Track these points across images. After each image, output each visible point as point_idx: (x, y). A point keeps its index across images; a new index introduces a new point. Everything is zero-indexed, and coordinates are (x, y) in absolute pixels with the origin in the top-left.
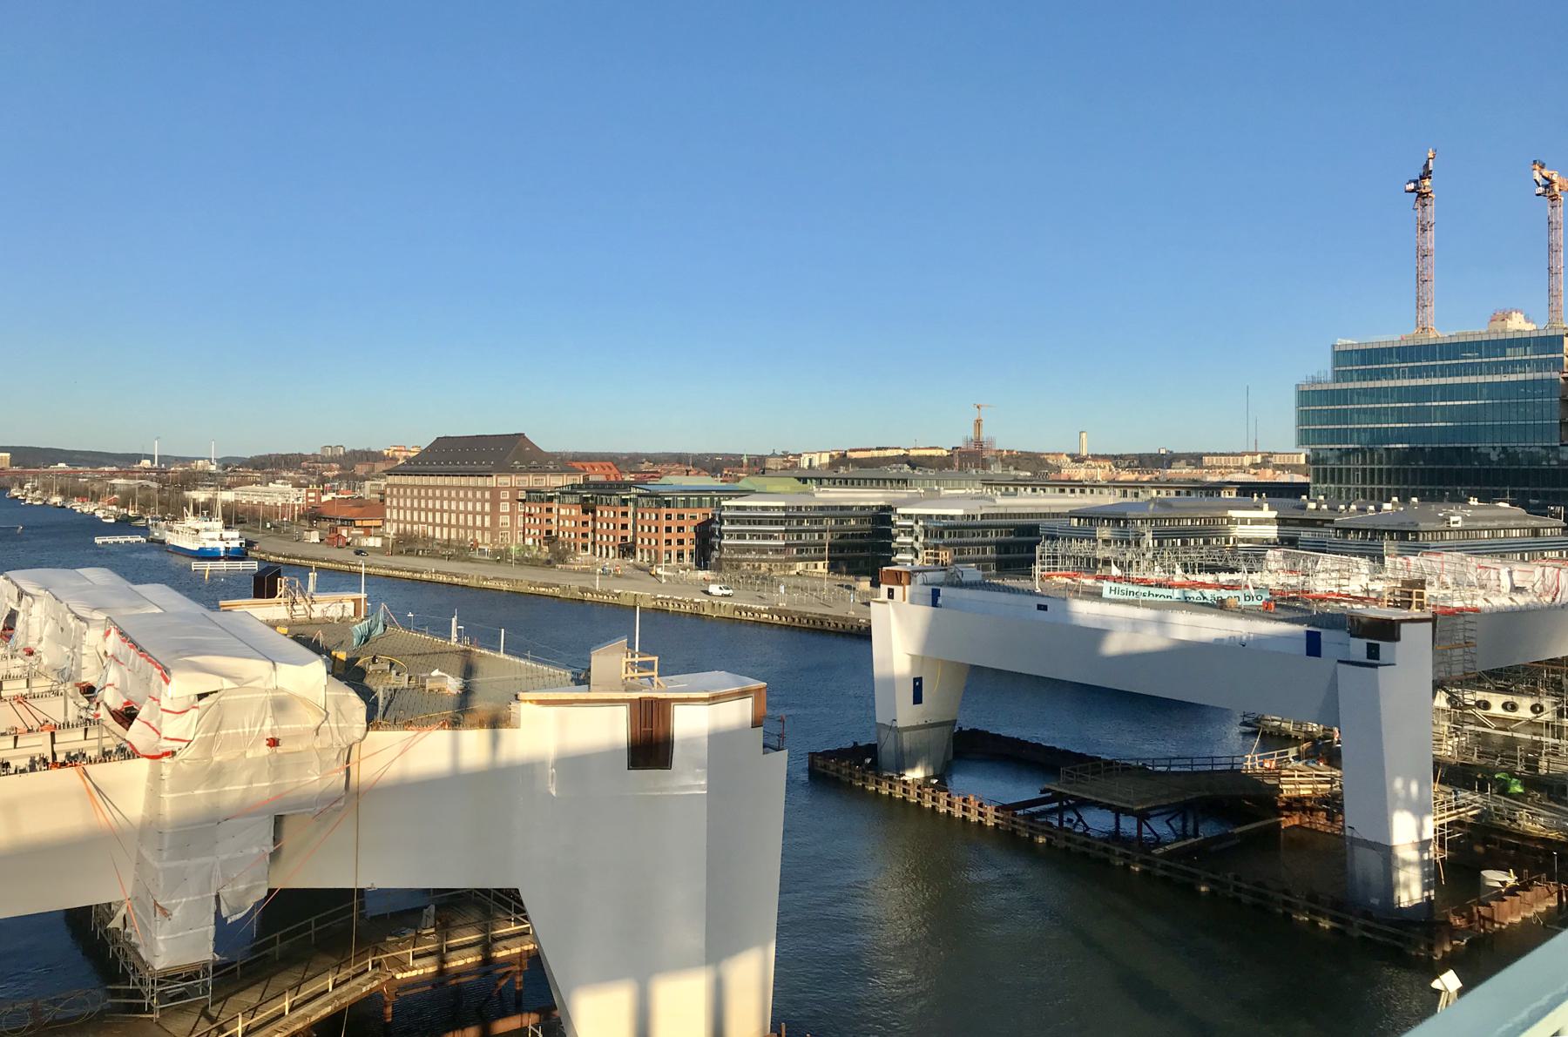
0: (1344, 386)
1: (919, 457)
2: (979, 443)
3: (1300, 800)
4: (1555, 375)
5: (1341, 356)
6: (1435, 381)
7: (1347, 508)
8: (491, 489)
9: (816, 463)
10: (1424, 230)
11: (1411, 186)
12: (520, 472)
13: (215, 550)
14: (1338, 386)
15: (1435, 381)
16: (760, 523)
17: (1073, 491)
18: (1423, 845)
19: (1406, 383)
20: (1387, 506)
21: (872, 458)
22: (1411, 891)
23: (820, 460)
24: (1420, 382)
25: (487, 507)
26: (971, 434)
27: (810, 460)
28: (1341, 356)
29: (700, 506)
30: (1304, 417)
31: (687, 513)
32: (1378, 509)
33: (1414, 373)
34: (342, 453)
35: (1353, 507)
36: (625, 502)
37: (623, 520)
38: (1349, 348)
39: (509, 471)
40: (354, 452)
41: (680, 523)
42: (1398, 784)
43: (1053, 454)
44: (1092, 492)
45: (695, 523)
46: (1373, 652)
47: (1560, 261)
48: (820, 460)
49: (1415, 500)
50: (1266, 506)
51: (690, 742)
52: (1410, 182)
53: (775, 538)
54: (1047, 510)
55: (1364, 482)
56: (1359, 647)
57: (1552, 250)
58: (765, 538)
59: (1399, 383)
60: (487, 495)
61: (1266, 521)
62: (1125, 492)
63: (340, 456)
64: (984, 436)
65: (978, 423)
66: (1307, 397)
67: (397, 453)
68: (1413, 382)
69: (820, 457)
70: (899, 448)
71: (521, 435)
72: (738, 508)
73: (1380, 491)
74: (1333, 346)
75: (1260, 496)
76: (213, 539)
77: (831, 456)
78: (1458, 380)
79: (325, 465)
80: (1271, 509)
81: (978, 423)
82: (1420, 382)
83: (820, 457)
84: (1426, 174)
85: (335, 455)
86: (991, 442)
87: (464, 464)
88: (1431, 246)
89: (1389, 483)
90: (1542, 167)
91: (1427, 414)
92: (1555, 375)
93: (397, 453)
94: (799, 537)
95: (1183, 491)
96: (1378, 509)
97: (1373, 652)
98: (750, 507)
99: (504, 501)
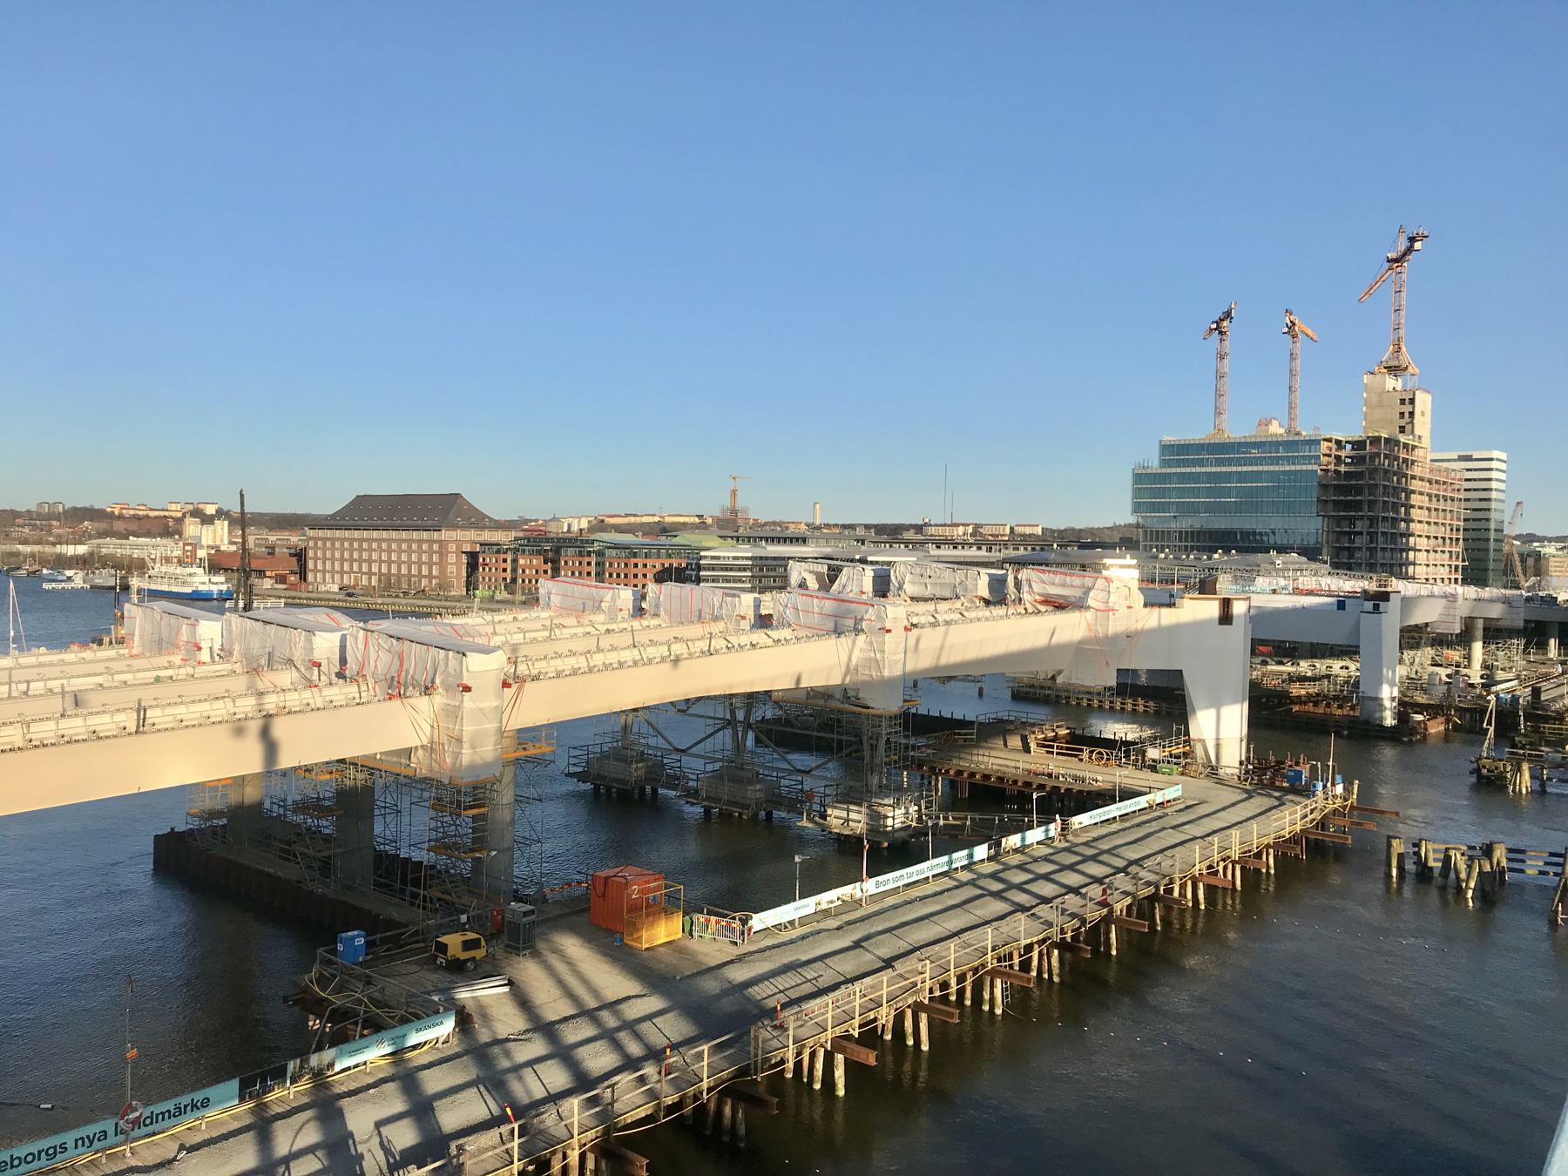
0: (1169, 470)
1: (673, 523)
2: (734, 512)
3: (1299, 697)
4: (1316, 467)
5: (1167, 449)
6: (1234, 469)
7: (1188, 557)
8: (440, 542)
9: (575, 528)
10: (1222, 358)
11: (1214, 326)
12: (463, 528)
13: (211, 593)
14: (1164, 471)
15: (1234, 469)
16: (731, 570)
17: (963, 548)
18: (1393, 699)
19: (1214, 469)
20: (1216, 556)
21: (629, 524)
22: (1389, 720)
23: (579, 524)
24: (1224, 469)
25: (435, 558)
26: (727, 503)
27: (569, 526)
28: (1167, 449)
29: (659, 557)
30: (1137, 493)
31: (649, 563)
32: (1210, 558)
33: (1219, 463)
34: (61, 509)
35: (1192, 557)
36: (589, 553)
37: (588, 569)
38: (1173, 443)
39: (454, 527)
40: (75, 509)
41: (645, 570)
42: (1385, 671)
43: (793, 523)
44: (963, 548)
45: (655, 571)
46: (1376, 607)
47: (1298, 382)
48: (579, 524)
49: (1234, 551)
50: (1128, 556)
51: (1239, 616)
52: (1213, 322)
53: (743, 582)
54: (962, 560)
55: (1180, 540)
56: (1369, 605)
57: (1292, 374)
58: (735, 581)
59: (1208, 469)
60: (435, 547)
61: (1129, 566)
62: (991, 548)
63: (59, 513)
64: (739, 505)
65: (734, 493)
66: (1139, 478)
67: (124, 511)
68: (1219, 469)
69: (579, 522)
70: (654, 515)
71: (458, 495)
72: (713, 558)
73: (1186, 546)
74: (1160, 441)
75: (1120, 549)
76: (204, 583)
77: (589, 522)
78: (1250, 469)
79: (44, 523)
80: (1132, 558)
81: (734, 493)
82: (1224, 469)
83: (579, 522)
84: (1228, 315)
85: (54, 512)
86: (745, 511)
87: (392, 519)
88: (1226, 370)
89: (1193, 541)
90: (1291, 314)
91: (1227, 492)
92: (1316, 467)
93: (124, 511)
94: (760, 581)
95: (1038, 548)
96: (1210, 558)
97: (1376, 607)
98: (724, 557)
99: (451, 552)
